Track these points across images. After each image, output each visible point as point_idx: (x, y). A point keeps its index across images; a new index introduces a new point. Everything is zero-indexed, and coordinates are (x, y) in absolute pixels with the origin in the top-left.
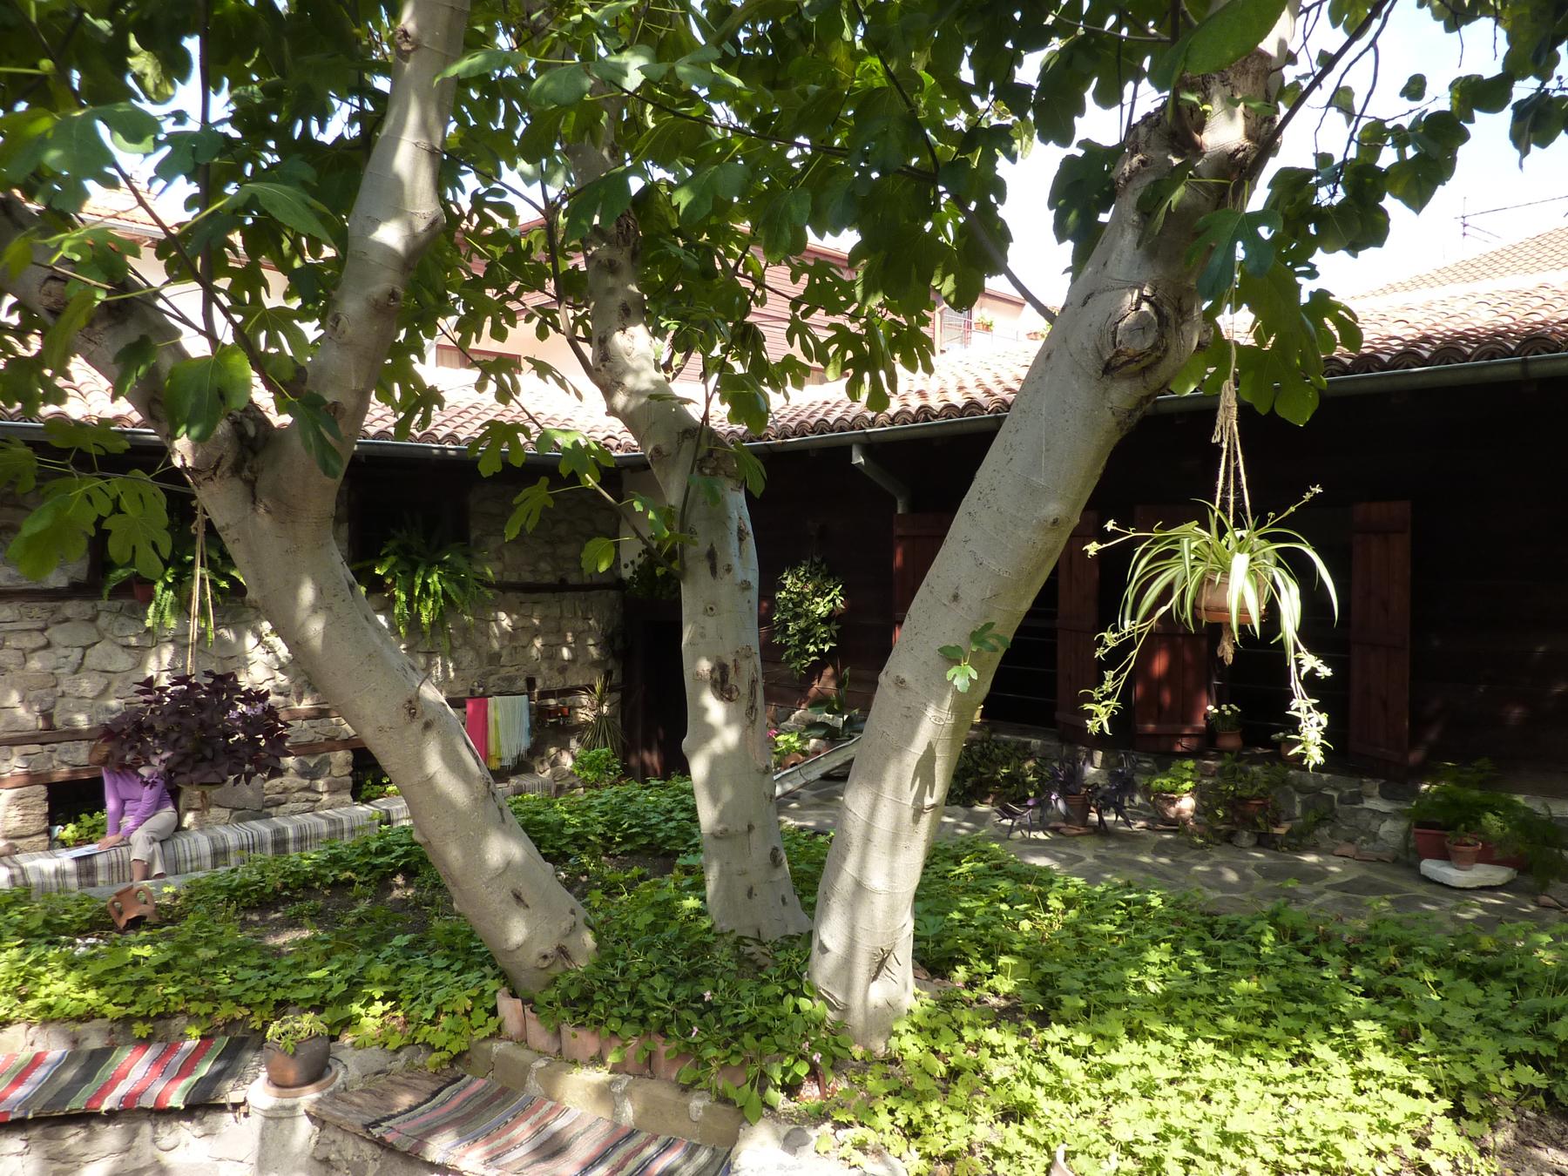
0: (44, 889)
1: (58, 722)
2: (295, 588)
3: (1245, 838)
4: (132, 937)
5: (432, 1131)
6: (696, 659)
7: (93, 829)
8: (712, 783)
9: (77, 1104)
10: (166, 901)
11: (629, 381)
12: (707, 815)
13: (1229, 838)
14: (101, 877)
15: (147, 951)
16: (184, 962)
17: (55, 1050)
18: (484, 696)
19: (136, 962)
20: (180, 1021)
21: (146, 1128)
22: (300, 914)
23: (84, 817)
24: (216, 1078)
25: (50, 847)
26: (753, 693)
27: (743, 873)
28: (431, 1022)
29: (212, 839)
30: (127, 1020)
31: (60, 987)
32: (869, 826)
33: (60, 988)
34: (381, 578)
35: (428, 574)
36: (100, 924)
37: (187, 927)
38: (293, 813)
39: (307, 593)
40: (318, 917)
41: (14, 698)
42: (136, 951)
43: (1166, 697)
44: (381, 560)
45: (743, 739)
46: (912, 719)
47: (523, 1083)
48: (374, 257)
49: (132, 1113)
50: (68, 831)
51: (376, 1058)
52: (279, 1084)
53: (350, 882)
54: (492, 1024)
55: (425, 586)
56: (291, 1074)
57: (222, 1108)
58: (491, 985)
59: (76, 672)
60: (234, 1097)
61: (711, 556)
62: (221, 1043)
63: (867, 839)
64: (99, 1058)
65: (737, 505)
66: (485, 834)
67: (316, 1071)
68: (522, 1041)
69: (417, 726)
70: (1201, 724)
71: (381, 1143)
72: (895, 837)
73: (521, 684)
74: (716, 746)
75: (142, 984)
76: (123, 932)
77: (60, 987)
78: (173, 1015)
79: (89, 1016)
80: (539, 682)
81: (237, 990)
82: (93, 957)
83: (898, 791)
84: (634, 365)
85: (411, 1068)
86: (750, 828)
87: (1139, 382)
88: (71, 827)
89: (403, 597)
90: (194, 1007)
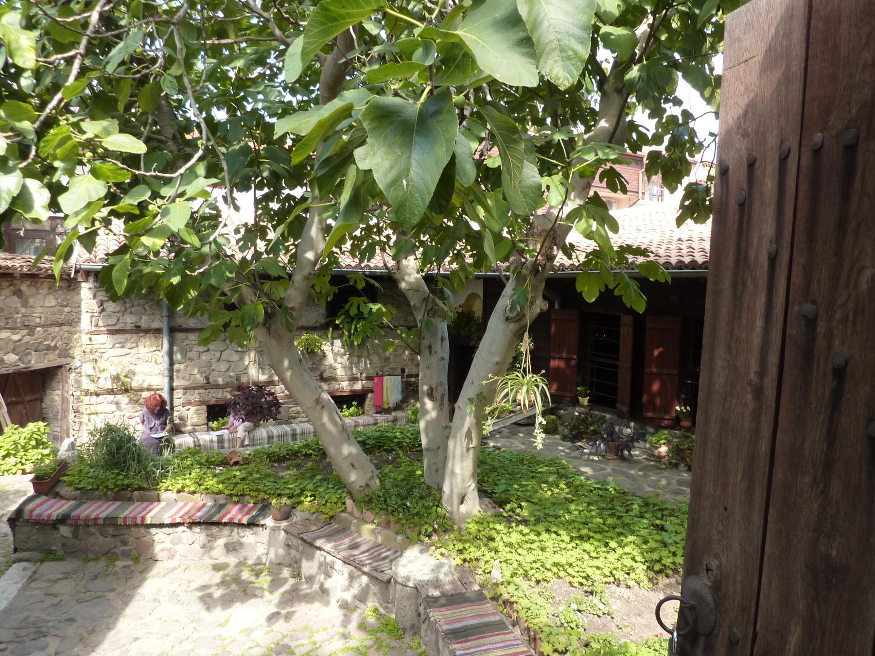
0: (205, 448)
1: (211, 381)
2: (282, 362)
3: (682, 466)
4: (234, 468)
5: (319, 538)
6: (422, 385)
7: (224, 424)
8: (426, 430)
9: (215, 519)
10: (246, 456)
11: (406, 278)
12: (424, 441)
13: (676, 466)
14: (226, 445)
15: (238, 473)
16: (249, 478)
17: (210, 503)
18: (382, 376)
19: (234, 477)
20: (247, 498)
21: (236, 530)
22: (291, 465)
23: (220, 419)
24: (257, 516)
25: (208, 431)
26: (442, 398)
27: (435, 464)
28: (324, 505)
29: (267, 432)
30: (231, 495)
31: (211, 483)
32: (454, 453)
33: (211, 482)
34: (338, 325)
35: (358, 323)
36: (224, 463)
37: (252, 465)
38: (301, 422)
39: (286, 363)
40: (298, 466)
41: (196, 371)
42: (235, 473)
43: (658, 401)
44: (338, 317)
45: (438, 415)
46: (463, 419)
47: (350, 528)
48: (304, 262)
49: (230, 524)
50: (215, 424)
51: (306, 515)
52: (275, 519)
53: (311, 454)
54: (343, 508)
55: (356, 328)
56: (279, 516)
57: (258, 525)
58: (344, 495)
59: (218, 361)
60: (262, 522)
61: (430, 347)
62: (260, 506)
63: (454, 457)
64: (222, 506)
65: (443, 328)
66: (342, 444)
67: (287, 517)
68: (352, 514)
69: (319, 407)
70: (674, 415)
71: (302, 539)
72: (462, 456)
73: (399, 371)
74: (428, 417)
75: (237, 483)
76: (231, 466)
77: (211, 483)
78: (245, 495)
79: (220, 493)
80: (407, 371)
81: (266, 489)
82: (221, 474)
83: (461, 442)
84: (409, 271)
85: (317, 519)
86: (439, 448)
87: (517, 324)
88: (215, 423)
89: (347, 333)
90: (252, 493)
